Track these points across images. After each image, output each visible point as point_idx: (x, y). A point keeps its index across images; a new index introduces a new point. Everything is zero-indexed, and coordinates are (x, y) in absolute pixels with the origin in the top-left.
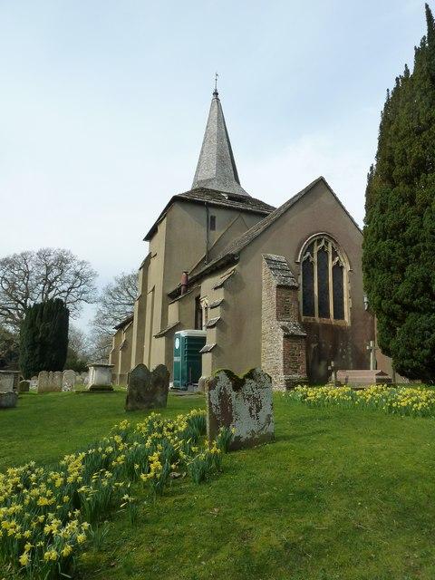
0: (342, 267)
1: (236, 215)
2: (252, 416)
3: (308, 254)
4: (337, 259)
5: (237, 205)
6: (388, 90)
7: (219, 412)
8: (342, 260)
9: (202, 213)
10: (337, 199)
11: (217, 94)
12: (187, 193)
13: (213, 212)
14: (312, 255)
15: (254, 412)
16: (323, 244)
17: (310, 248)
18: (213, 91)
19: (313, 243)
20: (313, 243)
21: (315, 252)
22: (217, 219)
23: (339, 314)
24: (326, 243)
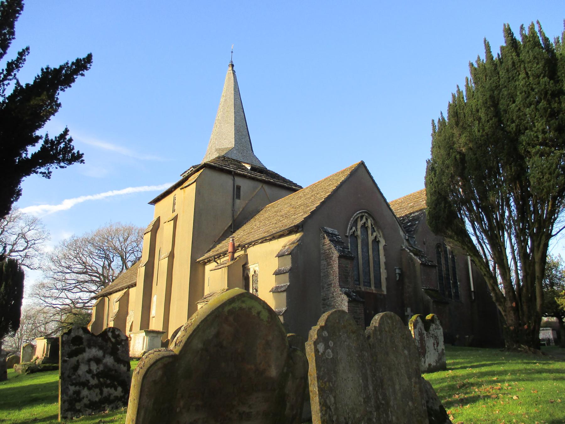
0: (379, 242)
1: (260, 185)
2: (435, 349)
3: (354, 228)
4: (375, 234)
5: (258, 175)
6: (433, 121)
7: (419, 346)
8: (378, 235)
9: (227, 180)
10: (373, 181)
11: (233, 66)
12: (212, 161)
13: (239, 181)
14: (357, 229)
15: (436, 346)
16: (364, 220)
17: (356, 222)
18: (229, 63)
19: (357, 219)
20: (357, 219)
21: (359, 227)
22: (242, 189)
23: (378, 284)
24: (367, 219)
